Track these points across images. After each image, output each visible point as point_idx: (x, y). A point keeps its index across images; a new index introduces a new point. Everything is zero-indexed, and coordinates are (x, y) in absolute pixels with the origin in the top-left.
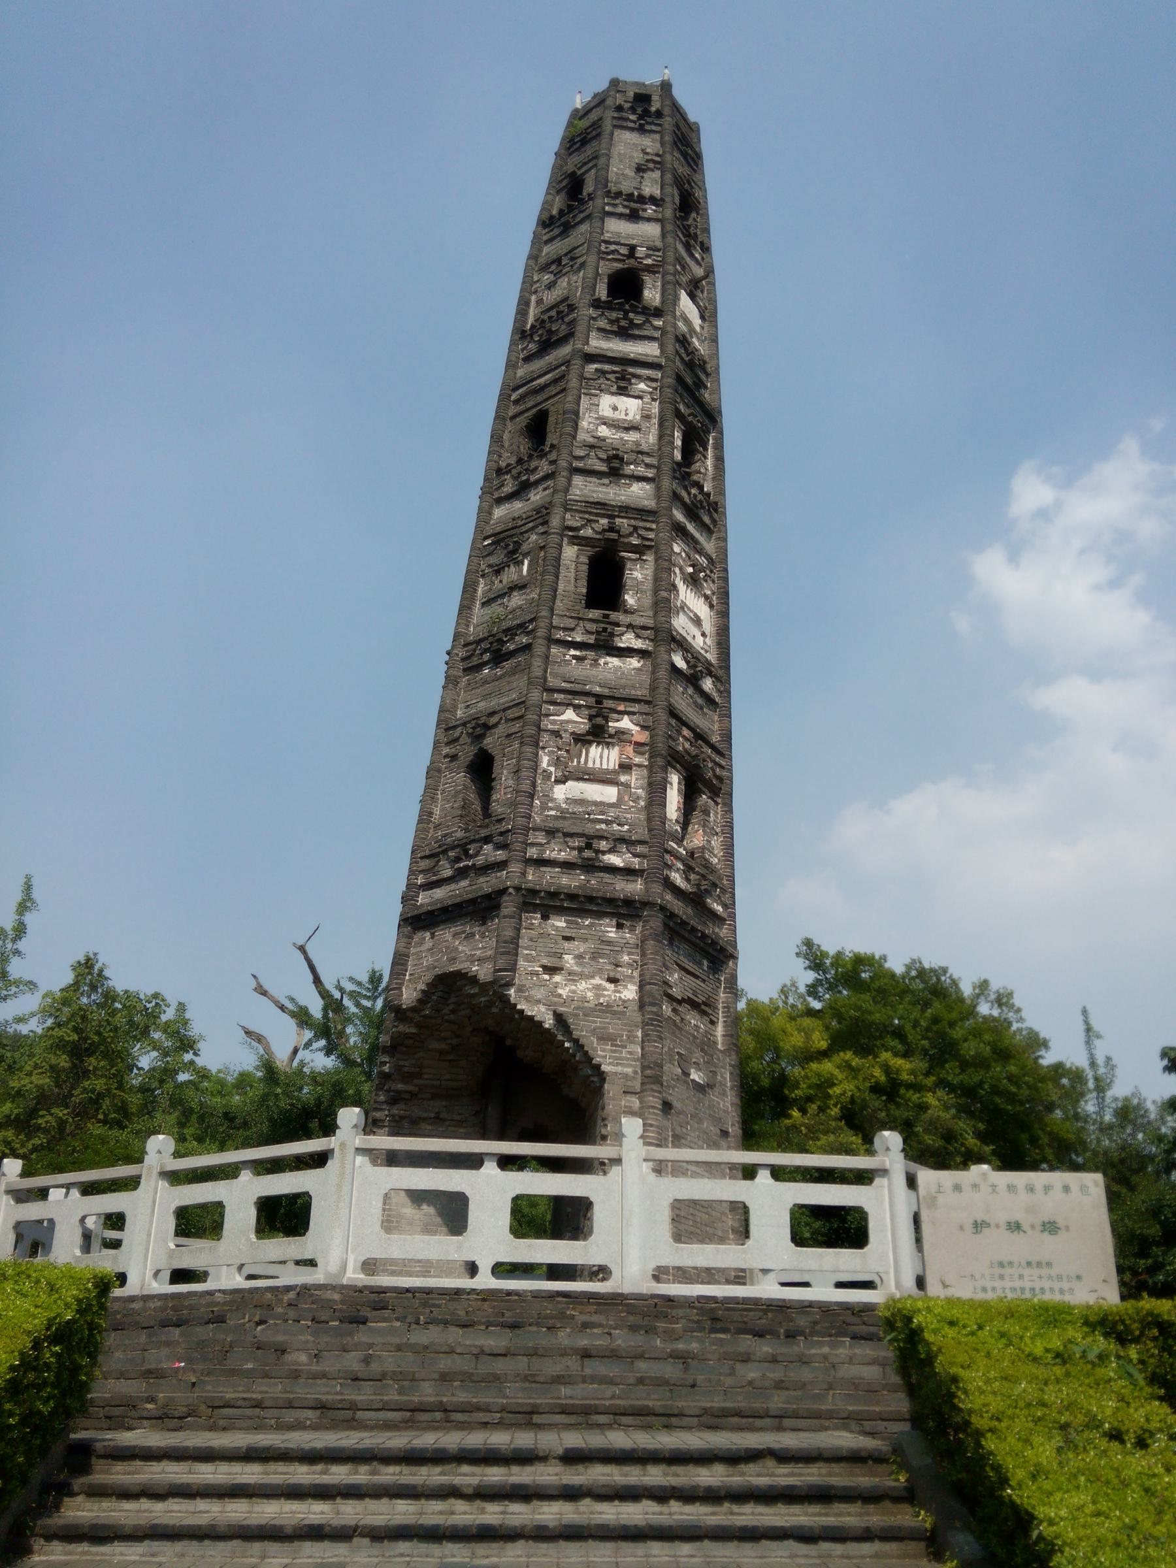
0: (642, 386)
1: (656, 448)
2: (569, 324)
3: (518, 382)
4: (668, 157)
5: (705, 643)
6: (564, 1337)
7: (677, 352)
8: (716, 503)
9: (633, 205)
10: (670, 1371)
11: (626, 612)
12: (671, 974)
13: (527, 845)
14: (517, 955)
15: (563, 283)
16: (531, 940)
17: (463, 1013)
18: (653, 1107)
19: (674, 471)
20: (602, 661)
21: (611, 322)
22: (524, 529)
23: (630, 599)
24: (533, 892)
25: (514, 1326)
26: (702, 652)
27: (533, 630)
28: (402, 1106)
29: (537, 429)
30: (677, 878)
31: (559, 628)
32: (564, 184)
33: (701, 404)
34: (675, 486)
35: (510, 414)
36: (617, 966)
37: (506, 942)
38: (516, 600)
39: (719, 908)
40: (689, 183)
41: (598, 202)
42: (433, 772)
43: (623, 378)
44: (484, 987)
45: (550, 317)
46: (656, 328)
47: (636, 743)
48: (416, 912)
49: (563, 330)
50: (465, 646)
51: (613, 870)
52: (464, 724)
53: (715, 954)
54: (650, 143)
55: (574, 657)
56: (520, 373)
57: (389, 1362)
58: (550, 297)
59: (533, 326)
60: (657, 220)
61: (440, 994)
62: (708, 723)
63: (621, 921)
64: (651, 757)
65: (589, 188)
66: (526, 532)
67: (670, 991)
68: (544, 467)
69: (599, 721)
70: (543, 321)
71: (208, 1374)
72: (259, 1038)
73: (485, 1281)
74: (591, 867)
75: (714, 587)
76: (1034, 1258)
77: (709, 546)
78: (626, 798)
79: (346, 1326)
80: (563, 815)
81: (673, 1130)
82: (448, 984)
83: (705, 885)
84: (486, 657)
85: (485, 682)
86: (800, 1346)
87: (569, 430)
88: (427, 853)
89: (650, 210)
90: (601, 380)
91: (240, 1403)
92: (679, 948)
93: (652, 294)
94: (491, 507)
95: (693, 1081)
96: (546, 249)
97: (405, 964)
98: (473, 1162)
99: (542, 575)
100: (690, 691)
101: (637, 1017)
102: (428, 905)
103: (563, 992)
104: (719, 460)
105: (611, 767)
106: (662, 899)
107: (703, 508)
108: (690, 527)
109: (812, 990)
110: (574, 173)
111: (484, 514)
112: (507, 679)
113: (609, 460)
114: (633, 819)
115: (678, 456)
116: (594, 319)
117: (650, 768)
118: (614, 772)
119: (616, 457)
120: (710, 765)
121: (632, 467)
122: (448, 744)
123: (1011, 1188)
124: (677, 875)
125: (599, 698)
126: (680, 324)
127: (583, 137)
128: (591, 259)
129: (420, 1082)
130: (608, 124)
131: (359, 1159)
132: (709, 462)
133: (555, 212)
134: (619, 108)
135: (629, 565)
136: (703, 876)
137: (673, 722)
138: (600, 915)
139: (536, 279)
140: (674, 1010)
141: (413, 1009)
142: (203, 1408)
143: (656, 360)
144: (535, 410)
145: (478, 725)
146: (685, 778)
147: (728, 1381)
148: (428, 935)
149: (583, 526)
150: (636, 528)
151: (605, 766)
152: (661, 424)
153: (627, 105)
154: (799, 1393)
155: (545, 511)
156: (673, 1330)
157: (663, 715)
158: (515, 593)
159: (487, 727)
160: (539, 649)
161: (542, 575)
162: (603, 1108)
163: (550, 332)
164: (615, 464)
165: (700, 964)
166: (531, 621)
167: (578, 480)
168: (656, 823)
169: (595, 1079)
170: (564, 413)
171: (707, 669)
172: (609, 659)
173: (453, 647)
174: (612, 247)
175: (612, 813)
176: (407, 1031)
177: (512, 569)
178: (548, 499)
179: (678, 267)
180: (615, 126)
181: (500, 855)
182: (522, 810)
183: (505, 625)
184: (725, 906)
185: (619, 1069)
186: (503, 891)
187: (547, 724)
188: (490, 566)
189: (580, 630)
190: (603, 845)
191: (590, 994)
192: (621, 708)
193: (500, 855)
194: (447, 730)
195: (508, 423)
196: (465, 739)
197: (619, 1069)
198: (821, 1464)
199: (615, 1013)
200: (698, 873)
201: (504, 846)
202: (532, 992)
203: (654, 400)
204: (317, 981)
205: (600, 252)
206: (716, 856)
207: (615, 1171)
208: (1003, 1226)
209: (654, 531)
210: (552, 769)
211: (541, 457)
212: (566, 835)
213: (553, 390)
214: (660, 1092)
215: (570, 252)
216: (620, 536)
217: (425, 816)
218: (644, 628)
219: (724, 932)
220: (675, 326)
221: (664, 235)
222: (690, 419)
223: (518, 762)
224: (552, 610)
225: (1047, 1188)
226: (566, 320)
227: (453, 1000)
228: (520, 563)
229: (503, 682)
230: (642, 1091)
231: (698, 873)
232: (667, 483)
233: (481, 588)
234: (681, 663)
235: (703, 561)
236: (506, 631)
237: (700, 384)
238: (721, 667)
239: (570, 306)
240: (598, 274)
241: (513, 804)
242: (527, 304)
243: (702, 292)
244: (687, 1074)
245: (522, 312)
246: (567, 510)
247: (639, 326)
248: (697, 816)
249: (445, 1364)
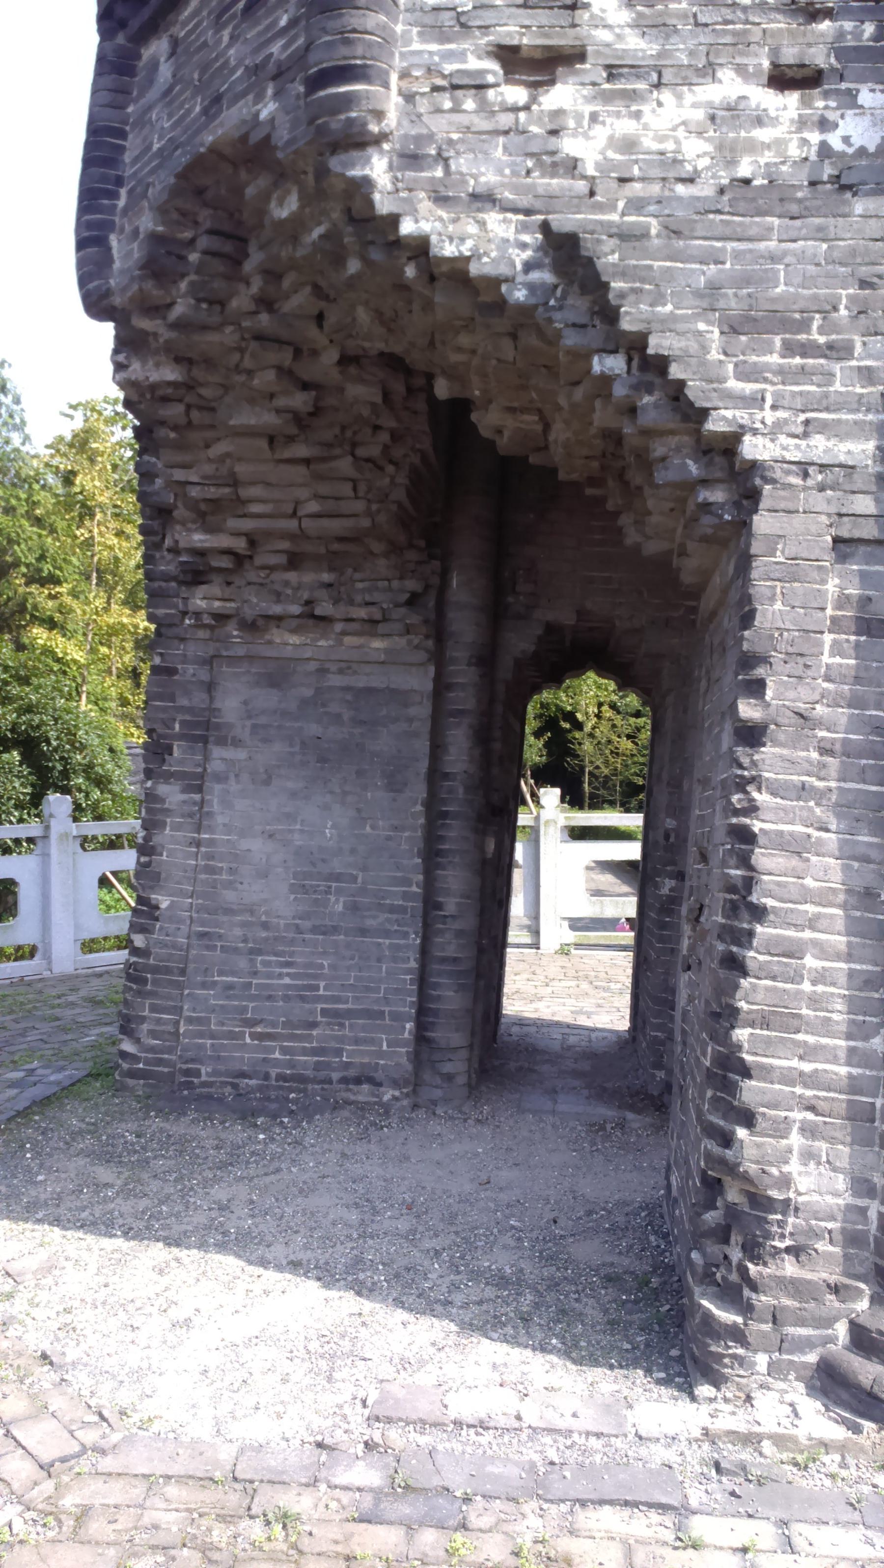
28: (215, 589)
61: (203, 242)
103: (586, 148)
129: (247, 525)
162: (747, 619)
169: (717, 495)
185: (819, 447)
191: (696, 151)
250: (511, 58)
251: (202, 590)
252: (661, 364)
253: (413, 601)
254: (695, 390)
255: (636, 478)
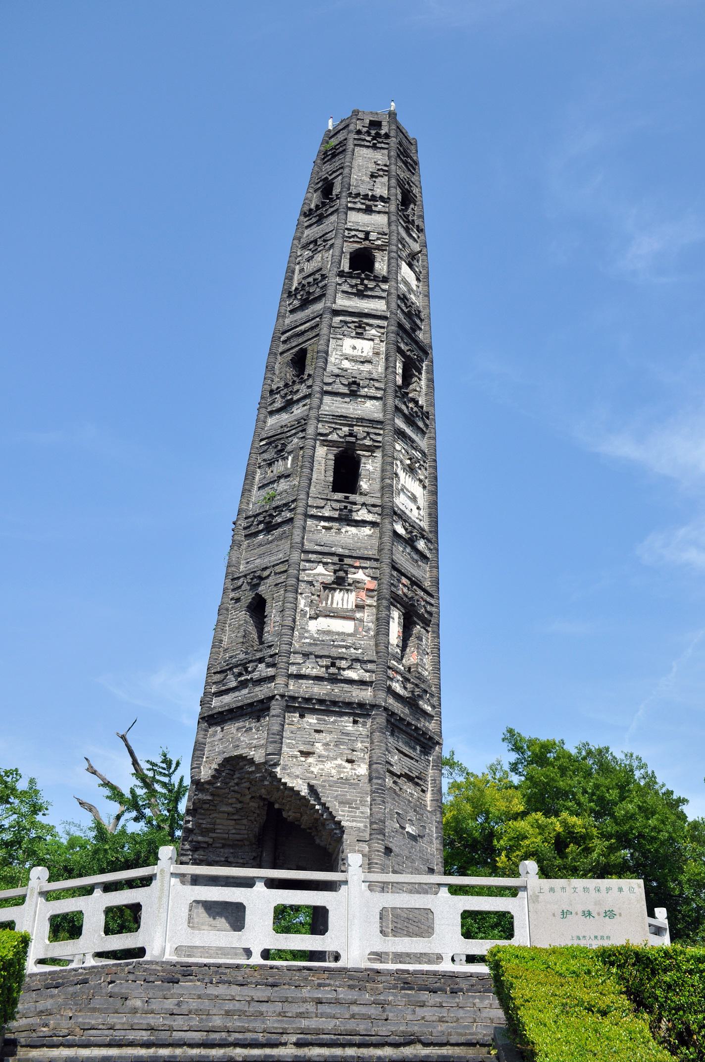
0: (373, 332)
1: (383, 376)
2: (322, 288)
3: (286, 328)
4: (393, 167)
5: (419, 514)
6: (305, 992)
7: (399, 306)
8: (428, 413)
9: (368, 202)
10: (373, 1011)
11: (361, 494)
12: (392, 757)
13: (289, 664)
14: (282, 743)
15: (318, 257)
16: (292, 732)
17: (244, 785)
18: (378, 851)
19: (396, 391)
20: (343, 530)
21: (352, 286)
22: (289, 434)
23: (364, 485)
24: (294, 698)
25: (273, 985)
26: (417, 521)
27: (294, 508)
29: (299, 361)
30: (397, 687)
31: (313, 507)
32: (319, 185)
33: (416, 342)
34: (397, 402)
35: (280, 351)
36: (353, 751)
37: (273, 734)
38: (283, 485)
39: (429, 709)
40: (409, 184)
41: (344, 201)
42: (222, 610)
43: (360, 327)
44: (258, 766)
45: (309, 283)
46: (383, 291)
47: (368, 590)
48: (210, 713)
49: (318, 292)
50: (246, 518)
51: (350, 682)
52: (245, 576)
53: (425, 741)
54: (381, 157)
55: (324, 527)
56: (287, 321)
57: (194, 1004)
58: (309, 267)
59: (296, 289)
60: (385, 213)
61: (227, 771)
62: (423, 573)
63: (356, 719)
64: (378, 600)
65: (336, 191)
66: (290, 436)
67: (391, 769)
68: (303, 390)
69: (341, 574)
70: (304, 285)
71: (80, 1011)
72: (90, 808)
73: (256, 959)
74: (334, 680)
75: (426, 473)
76: (599, 934)
77: (423, 443)
78: (360, 629)
79: (166, 984)
80: (315, 643)
81: (393, 867)
82: (233, 765)
83: (417, 692)
84: (261, 527)
85: (260, 545)
86: (460, 998)
87: (321, 364)
88: (219, 669)
89: (380, 206)
90: (345, 328)
91: (100, 1027)
92: (398, 738)
93: (381, 266)
94: (266, 417)
95: (407, 832)
96: (307, 232)
97: (203, 750)
98: (248, 883)
99: (301, 467)
100: (408, 550)
101: (368, 788)
102: (219, 707)
103: (315, 770)
104: (431, 380)
105: (350, 607)
106: (386, 702)
107: (418, 416)
108: (408, 431)
109: (514, 768)
110: (327, 178)
111: (261, 422)
112: (275, 543)
113: (349, 385)
114: (366, 645)
115: (399, 380)
116: (340, 285)
117: (378, 607)
118: (352, 610)
119: (354, 383)
120: (423, 603)
121: (366, 390)
122: (233, 590)
123: (586, 889)
124: (397, 685)
125: (341, 557)
126: (402, 286)
127: (333, 153)
128: (338, 242)
130: (350, 145)
131: (173, 880)
132: (423, 383)
133: (313, 206)
134: (359, 132)
135: (363, 460)
136: (417, 685)
137: (395, 573)
138: (341, 714)
139: (299, 254)
140: (395, 782)
141: (208, 783)
142: (78, 1030)
143: (383, 314)
144: (297, 349)
145: (255, 577)
146: (404, 614)
147: (409, 1017)
148: (219, 729)
149: (331, 433)
150: (368, 433)
151: (345, 607)
152: (387, 359)
153: (365, 130)
154: (454, 1024)
155: (303, 422)
156: (377, 988)
157: (387, 569)
158: (282, 481)
159: (261, 578)
160: (298, 522)
161: (301, 467)
163: (309, 293)
164: (354, 388)
165: (414, 749)
166: (293, 501)
167: (327, 399)
168: (382, 647)
169: (338, 832)
170: (318, 352)
171: (421, 533)
172: (348, 528)
173: (238, 519)
174: (353, 233)
175: (350, 641)
176: (205, 798)
177: (280, 462)
178: (306, 413)
179: (400, 246)
180: (355, 145)
181: (271, 671)
182: (286, 639)
183: (274, 504)
184: (433, 707)
185: (354, 824)
186: (272, 698)
187: (303, 576)
188: (264, 460)
189: (328, 508)
190: (344, 664)
191: (334, 772)
192: (357, 564)
193: (271, 671)
194: (233, 580)
195: (279, 357)
196: (246, 587)
197: (354, 824)
198: (449, 1047)
199: (352, 784)
200: (413, 683)
201: (273, 665)
202: (293, 770)
203: (382, 341)
204: (135, 763)
205: (344, 236)
206: (426, 670)
207: (343, 888)
208: (580, 914)
209: (384, 436)
210: (307, 609)
211: (301, 383)
212: (317, 657)
213: (311, 334)
214: (383, 840)
215: (323, 236)
216: (357, 439)
217: (217, 643)
218: (374, 506)
219: (432, 726)
220: (397, 289)
221: (389, 224)
222: (408, 353)
223: (283, 604)
224: (308, 494)
225: (608, 889)
226: (320, 285)
227: (237, 775)
228: (285, 459)
229: (273, 545)
230: (370, 840)
231: (413, 683)
232: (390, 401)
233: (258, 477)
234: (400, 530)
235: (418, 455)
236: (275, 508)
237: (416, 328)
238: (431, 532)
239: (322, 275)
240: (343, 252)
241: (280, 635)
242: (293, 272)
243: (418, 261)
244: (403, 828)
245: (289, 278)
246: (319, 421)
247: (372, 289)
248: (413, 641)
249: (229, 1006)
250: (301, 752)
251: (198, 853)
252: (328, 808)
253: (254, 858)
254: (334, 813)
255: (320, 828)
